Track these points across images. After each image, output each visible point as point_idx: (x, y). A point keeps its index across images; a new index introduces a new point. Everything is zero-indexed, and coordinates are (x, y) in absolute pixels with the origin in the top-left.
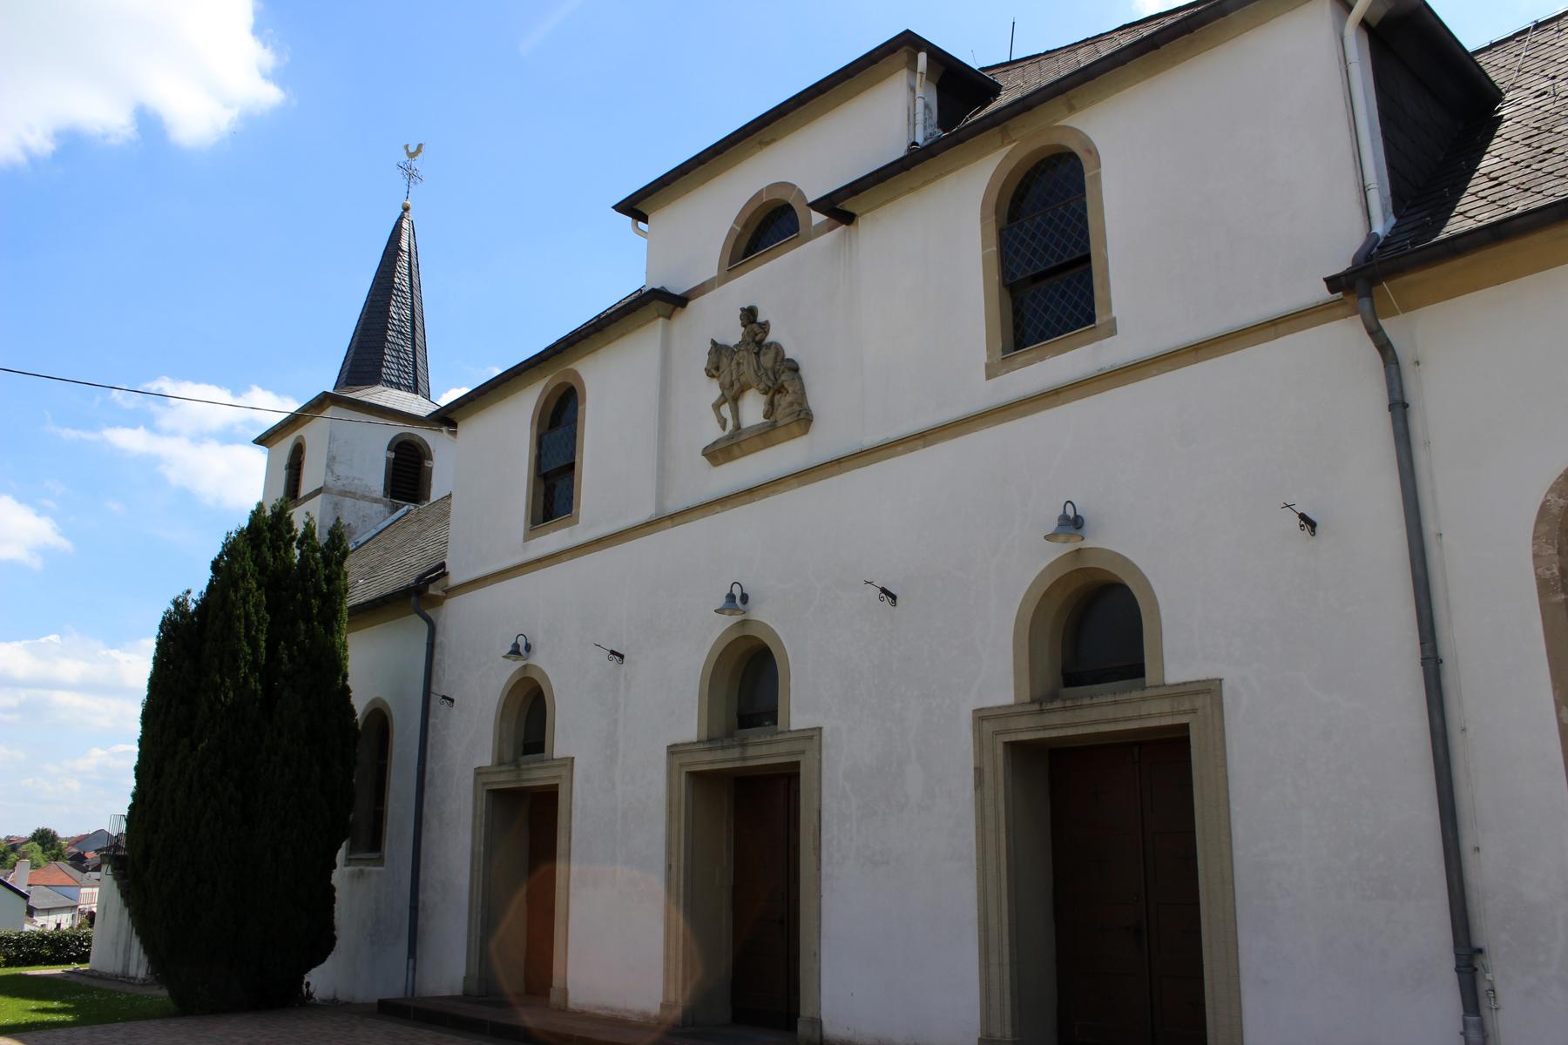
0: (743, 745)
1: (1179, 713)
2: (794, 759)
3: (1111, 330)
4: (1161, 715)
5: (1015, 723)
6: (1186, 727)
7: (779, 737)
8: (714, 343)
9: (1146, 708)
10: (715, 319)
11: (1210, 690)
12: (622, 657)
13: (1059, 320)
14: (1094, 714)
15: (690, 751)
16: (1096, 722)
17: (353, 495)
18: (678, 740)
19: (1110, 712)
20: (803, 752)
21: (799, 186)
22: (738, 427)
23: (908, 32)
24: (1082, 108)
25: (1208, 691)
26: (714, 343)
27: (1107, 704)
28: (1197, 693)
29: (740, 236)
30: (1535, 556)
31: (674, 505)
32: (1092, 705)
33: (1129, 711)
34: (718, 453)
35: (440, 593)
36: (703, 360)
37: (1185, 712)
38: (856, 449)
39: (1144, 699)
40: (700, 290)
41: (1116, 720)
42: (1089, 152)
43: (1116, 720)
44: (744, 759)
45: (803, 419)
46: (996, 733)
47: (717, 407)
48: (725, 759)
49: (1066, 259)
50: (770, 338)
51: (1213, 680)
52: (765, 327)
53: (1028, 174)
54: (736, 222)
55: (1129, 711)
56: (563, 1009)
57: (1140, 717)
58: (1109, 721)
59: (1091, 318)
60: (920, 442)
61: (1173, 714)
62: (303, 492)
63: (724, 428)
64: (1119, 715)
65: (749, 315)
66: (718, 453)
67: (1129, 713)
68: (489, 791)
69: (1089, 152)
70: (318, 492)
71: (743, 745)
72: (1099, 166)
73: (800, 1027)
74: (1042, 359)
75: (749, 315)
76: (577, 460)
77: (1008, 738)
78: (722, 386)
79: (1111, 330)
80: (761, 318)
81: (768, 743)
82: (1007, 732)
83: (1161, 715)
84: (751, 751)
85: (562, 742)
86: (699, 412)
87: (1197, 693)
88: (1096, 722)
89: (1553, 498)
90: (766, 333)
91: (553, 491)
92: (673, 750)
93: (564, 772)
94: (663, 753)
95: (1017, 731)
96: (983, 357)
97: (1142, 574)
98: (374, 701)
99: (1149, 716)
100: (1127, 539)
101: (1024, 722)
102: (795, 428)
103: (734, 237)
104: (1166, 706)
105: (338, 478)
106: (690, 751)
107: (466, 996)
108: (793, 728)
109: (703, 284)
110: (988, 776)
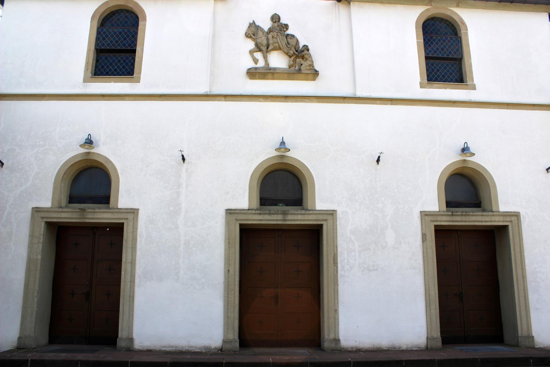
0: (285, 213)
1: (505, 221)
2: (319, 223)
3: (138, 81)
4: (499, 221)
5: (439, 218)
6: (123, 224)
7: (308, 212)
9: (493, 219)
13: (115, 70)
14: (474, 218)
15: (245, 214)
16: (474, 221)
18: (233, 207)
19: (480, 218)
20: (326, 220)
24: (461, 7)
25: (134, 213)
27: (479, 215)
28: (512, 216)
31: (216, 91)
32: (473, 215)
33: (487, 219)
36: (244, 28)
37: (508, 221)
38: (249, 93)
39: (493, 215)
41: (482, 221)
43: (482, 221)
44: (285, 220)
46: (432, 221)
47: (251, 52)
48: (69, 215)
49: (435, 55)
50: (289, 32)
51: (135, 209)
53: (112, 12)
55: (487, 219)
56: (130, 350)
57: (491, 221)
59: (132, 74)
60: (390, 102)
61: (503, 221)
64: (483, 220)
67: (247, 218)
68: (46, 222)
71: (285, 213)
74: (445, 88)
76: (138, 49)
77: (45, 220)
79: (138, 81)
81: (301, 214)
82: (437, 221)
83: (499, 221)
84: (290, 217)
87: (512, 216)
88: (474, 221)
90: (287, 29)
94: (223, 213)
95: (441, 221)
96: (419, 80)
97: (490, 174)
99: (495, 221)
100: (484, 159)
101: (444, 218)
102: (311, 76)
104: (501, 219)
106: (245, 214)
107: (19, 348)
108: (120, 206)
110: (428, 237)
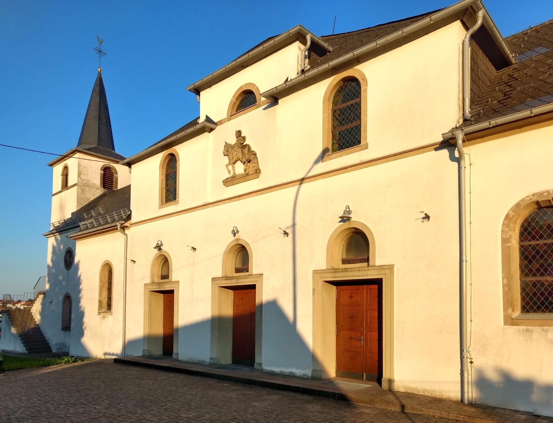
3: (366, 147)
8: (226, 143)
10: (225, 134)
11: (391, 268)
12: (135, 262)
17: (89, 186)
21: (257, 85)
22: (234, 173)
23: (278, 104)
26: (226, 143)
29: (234, 103)
30: (502, 231)
34: (228, 182)
35: (128, 225)
39: (368, 270)
40: (221, 122)
42: (364, 79)
45: (257, 172)
47: (227, 166)
52: (244, 138)
54: (233, 97)
57: (367, 275)
58: (356, 276)
59: (359, 142)
61: (378, 275)
62: (70, 184)
63: (230, 174)
65: (239, 133)
66: (228, 182)
69: (364, 79)
70: (75, 185)
72: (367, 85)
73: (255, 365)
75: (239, 133)
78: (229, 159)
79: (366, 147)
80: (243, 135)
82: (324, 278)
85: (174, 276)
86: (221, 167)
89: (511, 212)
91: (170, 193)
92: (213, 279)
93: (176, 285)
98: (106, 261)
101: (329, 275)
103: (232, 103)
104: (376, 272)
105: (83, 180)
109: (221, 120)
